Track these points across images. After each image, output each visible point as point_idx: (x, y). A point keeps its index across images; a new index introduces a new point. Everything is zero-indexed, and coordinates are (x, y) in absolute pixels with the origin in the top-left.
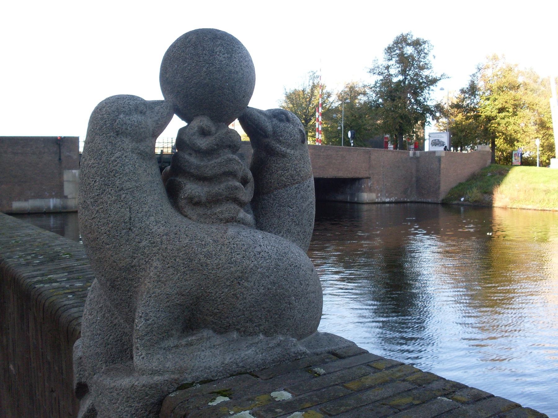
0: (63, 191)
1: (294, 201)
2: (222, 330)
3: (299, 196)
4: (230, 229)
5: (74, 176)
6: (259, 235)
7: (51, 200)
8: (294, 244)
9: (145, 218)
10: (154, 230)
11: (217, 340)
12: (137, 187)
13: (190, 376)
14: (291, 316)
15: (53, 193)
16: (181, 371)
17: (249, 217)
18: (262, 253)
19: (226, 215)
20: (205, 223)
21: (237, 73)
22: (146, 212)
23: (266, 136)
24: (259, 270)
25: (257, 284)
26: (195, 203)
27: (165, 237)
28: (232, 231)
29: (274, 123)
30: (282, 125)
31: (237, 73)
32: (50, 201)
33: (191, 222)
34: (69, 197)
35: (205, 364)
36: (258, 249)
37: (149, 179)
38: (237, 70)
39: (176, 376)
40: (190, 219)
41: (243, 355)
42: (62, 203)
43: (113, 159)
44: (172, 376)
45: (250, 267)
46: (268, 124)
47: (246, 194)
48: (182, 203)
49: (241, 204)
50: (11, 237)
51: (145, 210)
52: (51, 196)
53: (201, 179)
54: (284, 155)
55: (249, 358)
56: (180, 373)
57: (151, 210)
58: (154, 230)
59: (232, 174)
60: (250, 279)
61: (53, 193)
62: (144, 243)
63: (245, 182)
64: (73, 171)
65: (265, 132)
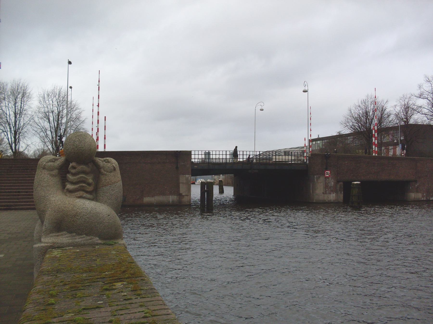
0: (179, 190)
11: (68, 235)
16: (54, 243)
19: (79, 195)
36: (84, 206)
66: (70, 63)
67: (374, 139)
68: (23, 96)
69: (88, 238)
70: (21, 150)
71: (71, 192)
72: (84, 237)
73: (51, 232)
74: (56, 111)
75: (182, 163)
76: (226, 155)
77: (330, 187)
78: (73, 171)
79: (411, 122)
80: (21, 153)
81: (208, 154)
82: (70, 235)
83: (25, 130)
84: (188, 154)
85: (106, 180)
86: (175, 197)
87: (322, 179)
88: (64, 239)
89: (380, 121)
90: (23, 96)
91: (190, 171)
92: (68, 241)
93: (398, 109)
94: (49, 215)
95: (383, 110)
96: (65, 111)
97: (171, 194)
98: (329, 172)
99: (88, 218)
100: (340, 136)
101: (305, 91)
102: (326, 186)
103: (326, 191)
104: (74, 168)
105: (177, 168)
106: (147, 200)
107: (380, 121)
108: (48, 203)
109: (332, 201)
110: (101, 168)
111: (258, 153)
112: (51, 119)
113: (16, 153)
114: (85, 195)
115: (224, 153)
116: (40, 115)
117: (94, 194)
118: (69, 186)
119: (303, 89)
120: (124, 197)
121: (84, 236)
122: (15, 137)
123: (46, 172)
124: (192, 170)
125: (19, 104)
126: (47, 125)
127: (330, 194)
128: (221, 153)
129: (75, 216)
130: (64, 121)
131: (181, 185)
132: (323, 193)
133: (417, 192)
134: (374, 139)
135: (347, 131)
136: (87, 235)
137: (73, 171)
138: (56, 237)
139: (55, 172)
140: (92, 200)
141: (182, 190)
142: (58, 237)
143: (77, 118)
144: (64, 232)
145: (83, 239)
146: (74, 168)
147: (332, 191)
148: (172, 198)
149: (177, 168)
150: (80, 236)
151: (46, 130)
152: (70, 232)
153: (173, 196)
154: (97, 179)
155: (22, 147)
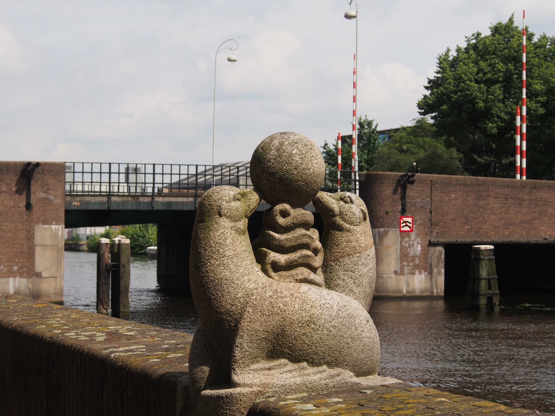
0: (33, 264)
1: (356, 267)
2: (295, 360)
3: (360, 263)
4: (302, 287)
5: (55, 236)
6: (325, 291)
7: (11, 279)
8: (356, 301)
9: (241, 277)
10: (247, 286)
11: (291, 366)
12: (235, 254)
13: (271, 390)
14: (349, 354)
15: (16, 268)
16: (265, 385)
17: (319, 277)
18: (326, 305)
19: (300, 277)
20: (284, 282)
21: (309, 169)
22: (242, 273)
23: (335, 216)
24: (323, 317)
25: (321, 327)
26: (276, 267)
27: (255, 291)
28: (305, 287)
29: (340, 204)
30: (347, 206)
31: (309, 169)
32: (8, 282)
33: (273, 281)
34: (44, 275)
35: (282, 383)
36: (324, 302)
37: (243, 249)
38: (309, 167)
39: (261, 389)
40: (273, 279)
41: (310, 379)
42: (31, 286)
43: (218, 234)
44: (258, 389)
45: (316, 314)
46: (335, 205)
47: (318, 261)
48: (269, 267)
49: (314, 270)
50: (42, 318)
51: (241, 271)
52: (11, 274)
53: (282, 250)
54: (348, 231)
55: (315, 382)
56: (264, 387)
57: (245, 271)
58: (247, 286)
59: (306, 246)
60: (316, 323)
61: (16, 268)
62: (240, 295)
63: (316, 251)
64: (53, 227)
65: (332, 211)
67: (518, 138)
69: (333, 371)
71: (276, 267)
72: (324, 371)
75: (43, 195)
76: (110, 173)
77: (413, 258)
81: (131, 171)
82: (295, 366)
85: (348, 241)
86: (24, 281)
88: (284, 375)
91: (63, 215)
92: (293, 380)
98: (410, 220)
99: (334, 327)
101: (348, 17)
102: (404, 256)
103: (402, 268)
104: (284, 214)
105: (29, 206)
108: (240, 295)
109: (418, 293)
110: (335, 216)
111: (193, 171)
115: (105, 168)
121: (325, 367)
124: (67, 212)
127: (413, 274)
128: (96, 168)
129: (310, 322)
131: (38, 251)
132: (396, 272)
134: (518, 138)
138: (267, 372)
139: (243, 224)
142: (272, 372)
144: (283, 361)
145: (324, 375)
147: (417, 267)
149: (29, 206)
150: (316, 369)
153: (17, 279)
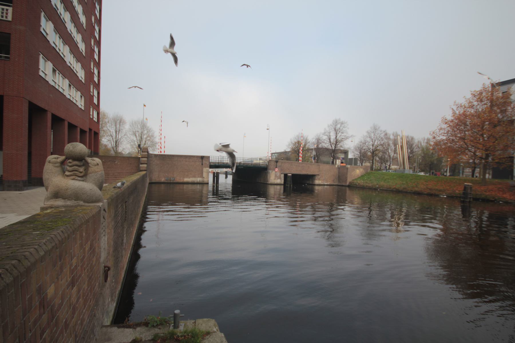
16: (52, 205)
66: (145, 105)
68: (120, 122)
70: (120, 151)
71: (67, 176)
73: (51, 198)
74: (140, 131)
78: (70, 164)
79: (320, 146)
80: (120, 153)
83: (122, 140)
84: (208, 157)
87: (274, 172)
89: (305, 145)
90: (120, 122)
93: (314, 140)
94: (51, 189)
95: (306, 140)
96: (146, 132)
97: (198, 177)
100: (285, 153)
102: (276, 176)
104: (70, 163)
106: (186, 180)
107: (305, 145)
112: (137, 135)
113: (116, 152)
114: (77, 178)
116: (130, 133)
117: (84, 176)
118: (67, 173)
119: (267, 128)
120: (339, 173)
122: (116, 144)
123: (51, 165)
125: (118, 126)
126: (135, 139)
129: (67, 190)
130: (145, 137)
133: (319, 180)
135: (289, 150)
136: (75, 200)
137: (70, 164)
139: (58, 165)
140: (83, 181)
141: (205, 175)
143: (153, 136)
146: (70, 163)
148: (199, 180)
151: (134, 141)
152: (64, 199)
154: (86, 170)
155: (120, 149)
